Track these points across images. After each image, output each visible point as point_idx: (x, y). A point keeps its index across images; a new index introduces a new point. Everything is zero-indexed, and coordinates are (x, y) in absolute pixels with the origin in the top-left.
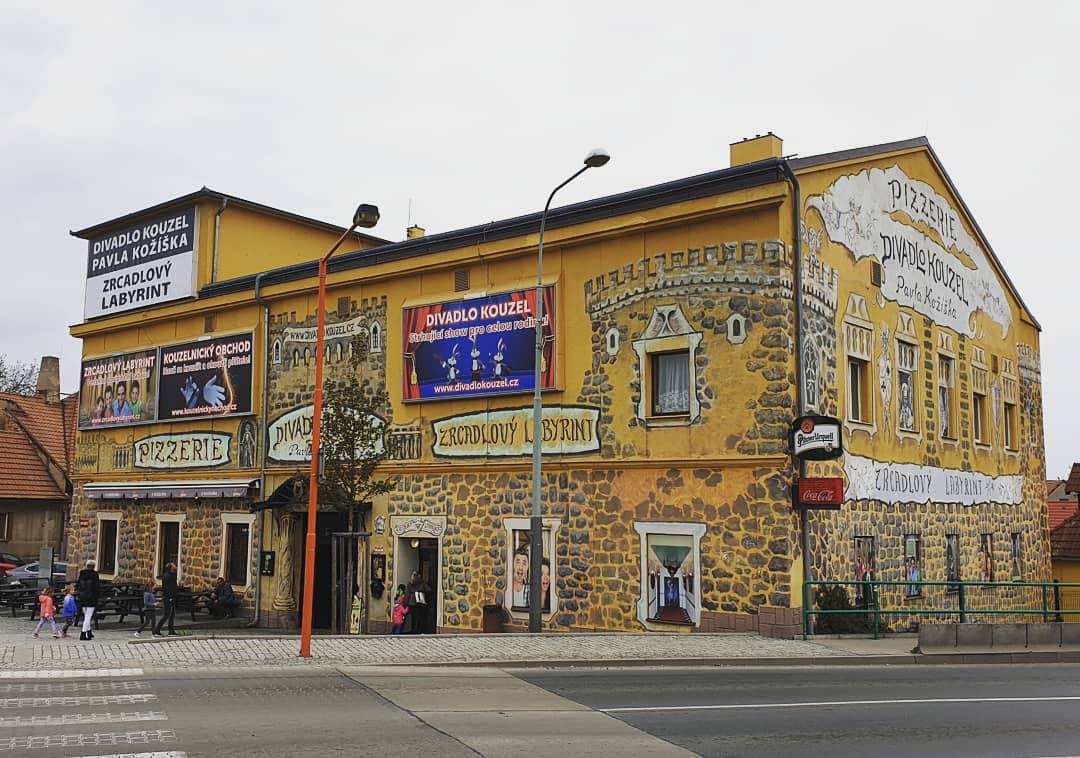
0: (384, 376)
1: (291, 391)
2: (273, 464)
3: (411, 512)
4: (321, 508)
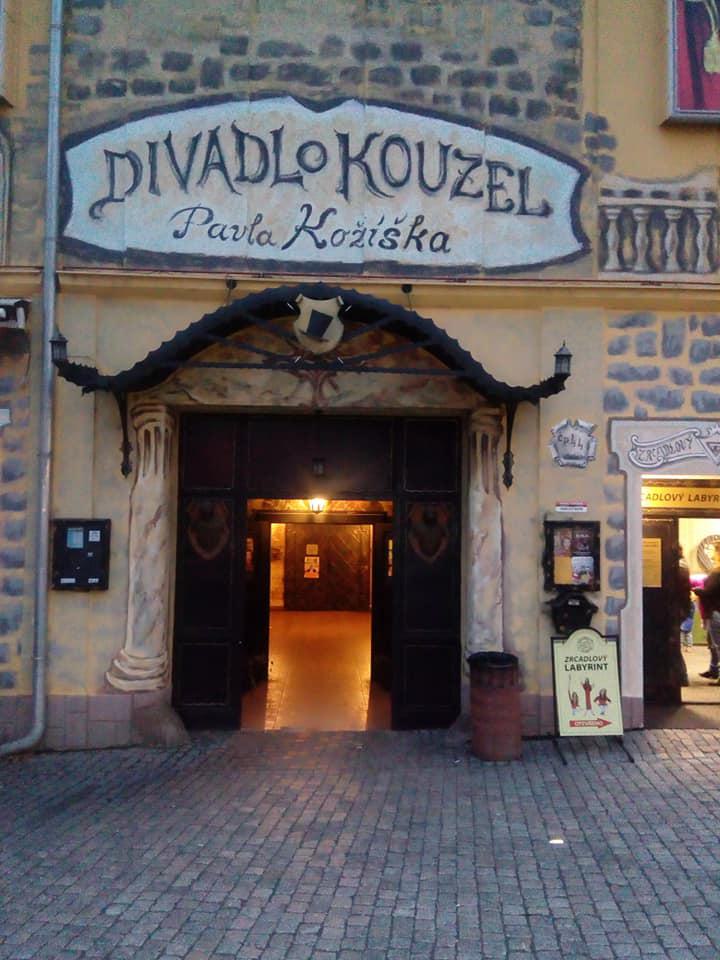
0: (574, 43)
1: (179, 48)
2: (87, 258)
3: (687, 410)
4: (332, 507)
